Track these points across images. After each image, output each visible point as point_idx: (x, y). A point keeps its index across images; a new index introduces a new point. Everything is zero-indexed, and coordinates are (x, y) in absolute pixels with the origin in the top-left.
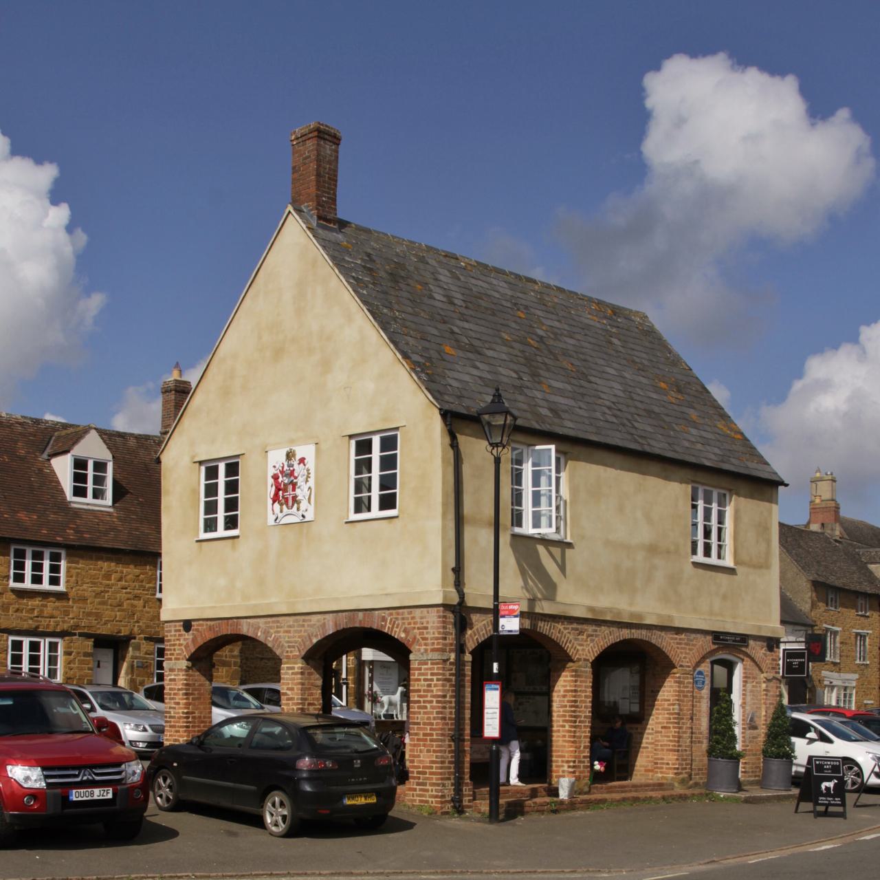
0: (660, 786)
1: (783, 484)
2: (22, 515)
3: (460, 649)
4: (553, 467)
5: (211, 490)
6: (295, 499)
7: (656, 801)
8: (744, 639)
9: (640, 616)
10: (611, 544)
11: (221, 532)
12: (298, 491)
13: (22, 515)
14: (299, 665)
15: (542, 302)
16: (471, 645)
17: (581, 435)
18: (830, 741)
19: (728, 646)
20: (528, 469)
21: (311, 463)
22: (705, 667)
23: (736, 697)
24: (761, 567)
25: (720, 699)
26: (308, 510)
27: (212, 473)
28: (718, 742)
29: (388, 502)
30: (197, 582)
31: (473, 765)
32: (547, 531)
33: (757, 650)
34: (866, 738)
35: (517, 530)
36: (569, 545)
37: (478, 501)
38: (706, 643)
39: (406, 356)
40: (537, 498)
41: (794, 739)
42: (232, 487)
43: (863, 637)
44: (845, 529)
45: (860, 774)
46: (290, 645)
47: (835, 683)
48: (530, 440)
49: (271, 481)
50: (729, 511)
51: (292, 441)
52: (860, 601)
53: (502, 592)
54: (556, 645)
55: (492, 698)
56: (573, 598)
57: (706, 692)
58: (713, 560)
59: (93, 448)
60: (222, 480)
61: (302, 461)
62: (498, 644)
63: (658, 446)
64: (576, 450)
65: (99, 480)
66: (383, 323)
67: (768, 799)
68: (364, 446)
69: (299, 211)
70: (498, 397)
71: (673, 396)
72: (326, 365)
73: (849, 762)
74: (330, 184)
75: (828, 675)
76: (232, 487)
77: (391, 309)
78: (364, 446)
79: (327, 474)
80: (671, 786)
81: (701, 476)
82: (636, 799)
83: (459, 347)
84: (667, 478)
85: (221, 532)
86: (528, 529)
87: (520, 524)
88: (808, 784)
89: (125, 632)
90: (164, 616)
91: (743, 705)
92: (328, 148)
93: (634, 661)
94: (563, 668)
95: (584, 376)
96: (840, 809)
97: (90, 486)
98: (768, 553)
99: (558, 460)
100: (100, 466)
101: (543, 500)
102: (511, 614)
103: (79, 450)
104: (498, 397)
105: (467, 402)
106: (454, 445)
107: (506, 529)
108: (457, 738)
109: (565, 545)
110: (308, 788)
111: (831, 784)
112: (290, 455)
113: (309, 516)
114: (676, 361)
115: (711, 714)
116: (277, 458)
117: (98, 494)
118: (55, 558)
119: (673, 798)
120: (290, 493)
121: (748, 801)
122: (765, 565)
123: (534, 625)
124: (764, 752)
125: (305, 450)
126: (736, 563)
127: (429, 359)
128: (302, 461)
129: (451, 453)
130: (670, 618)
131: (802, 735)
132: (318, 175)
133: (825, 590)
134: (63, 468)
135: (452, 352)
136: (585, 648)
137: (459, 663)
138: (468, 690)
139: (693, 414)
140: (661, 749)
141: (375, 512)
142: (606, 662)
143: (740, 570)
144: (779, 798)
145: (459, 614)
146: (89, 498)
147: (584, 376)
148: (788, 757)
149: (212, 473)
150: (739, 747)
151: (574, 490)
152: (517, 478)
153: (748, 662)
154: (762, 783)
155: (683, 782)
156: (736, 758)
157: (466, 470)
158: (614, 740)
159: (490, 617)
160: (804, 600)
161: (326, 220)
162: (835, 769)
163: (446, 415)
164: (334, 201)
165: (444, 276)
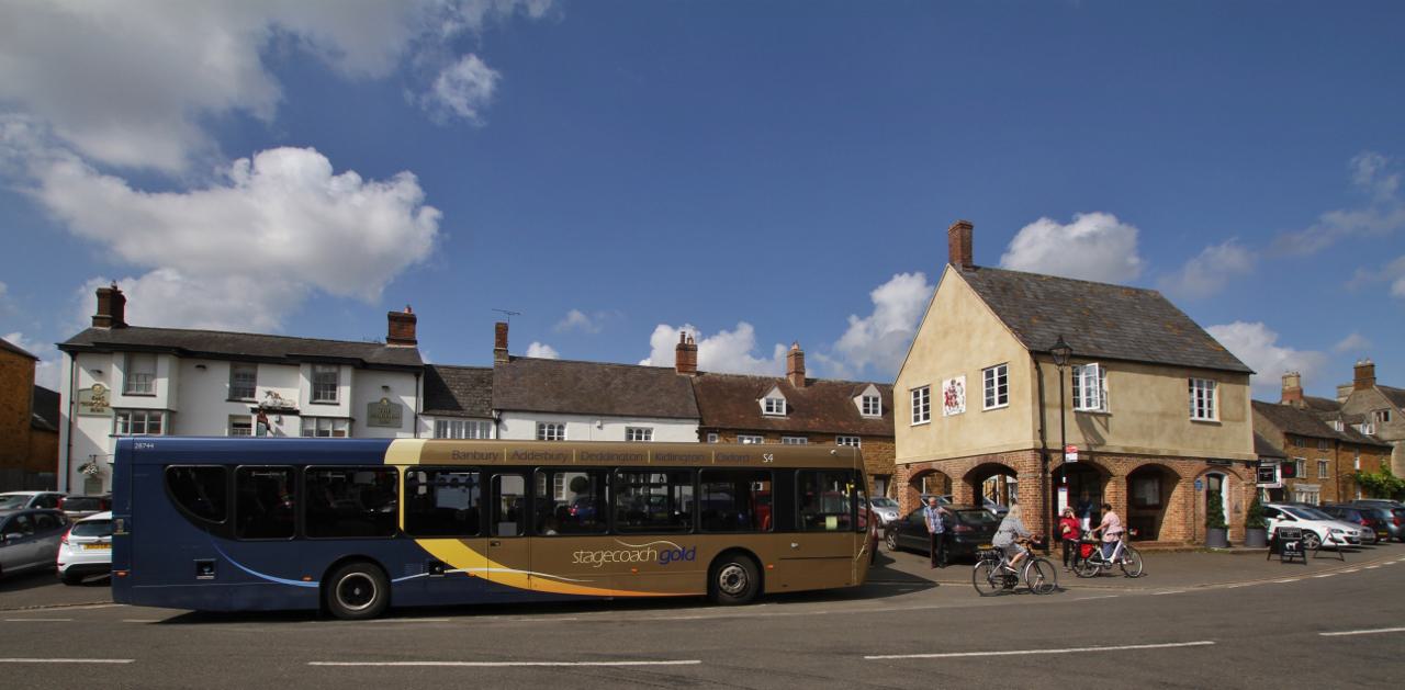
0: (1173, 544)
1: (1252, 372)
2: (841, 424)
3: (1045, 471)
4: (1097, 374)
5: (917, 402)
6: (956, 403)
7: (1171, 551)
8: (1229, 462)
9: (1156, 451)
10: (1134, 412)
11: (922, 421)
12: (958, 399)
13: (841, 424)
14: (961, 482)
15: (1091, 292)
16: (1051, 469)
17: (1115, 357)
18: (1295, 520)
19: (1218, 467)
20: (1082, 378)
21: (963, 386)
22: (1203, 478)
23: (1224, 495)
24: (1238, 421)
25: (1214, 498)
26: (963, 407)
27: (917, 394)
28: (1212, 520)
29: (1003, 400)
30: (912, 446)
31: (703, 514)
32: (1095, 408)
33: (1240, 469)
34: (1323, 518)
35: (1077, 409)
36: (1110, 415)
37: (1052, 395)
38: (1203, 465)
39: (1009, 326)
40: (1088, 394)
41: (1269, 519)
42: (926, 400)
43: (1324, 463)
44: (1308, 403)
45: (1318, 539)
46: (957, 472)
47: (1303, 489)
48: (1082, 362)
49: (944, 395)
50: (1215, 393)
51: (954, 375)
52: (1320, 443)
53: (1067, 441)
54: (1103, 467)
55: (1063, 496)
56: (1114, 443)
57: (1203, 492)
58: (1205, 418)
59: (872, 392)
60: (921, 397)
61: (959, 384)
62: (1068, 468)
63: (1165, 358)
64: (1110, 365)
65: (875, 406)
66: (997, 312)
67: (1248, 552)
68: (990, 374)
69: (953, 265)
70: (1061, 339)
71: (1175, 332)
72: (969, 337)
73: (1311, 533)
74: (1027, 285)
75: (1297, 486)
76: (926, 400)
77: (1001, 304)
78: (990, 374)
79: (971, 388)
80: (1181, 544)
81: (1194, 373)
82: (1157, 551)
83: (1040, 318)
84: (1171, 376)
85: (922, 421)
86: (1083, 408)
87: (1079, 406)
88: (1277, 544)
89: (888, 472)
90: (897, 462)
91: (1230, 499)
92: (967, 232)
93: (1153, 477)
94: (1109, 480)
95: (1118, 327)
96: (1302, 559)
97: (871, 408)
98: (1244, 413)
99: (1100, 372)
100: (875, 399)
101: (1093, 392)
102: (1072, 451)
103: (865, 393)
104: (1061, 339)
105: (1044, 346)
106: (1038, 368)
107: (1070, 408)
108: (1044, 516)
109: (1107, 415)
110: (958, 540)
111: (1294, 544)
112: (953, 382)
113: (964, 410)
114: (1177, 313)
115: (1207, 505)
116: (947, 385)
117: (875, 412)
118: (856, 441)
119: (1182, 550)
120: (953, 401)
121: (1233, 553)
122: (1243, 420)
123: (1091, 458)
124: (1246, 526)
125: (961, 379)
126: (1221, 419)
127: (1024, 327)
128: (959, 384)
129: (1036, 372)
130: (1177, 451)
131: (1274, 517)
132: (962, 246)
133: (1292, 437)
134: (859, 401)
135: (1036, 321)
136: (1122, 469)
137: (1044, 479)
138: (1050, 492)
139: (1189, 340)
140: (1174, 523)
141: (997, 405)
142: (1136, 479)
143: (1224, 423)
144: (1257, 552)
145: (1044, 453)
146: (871, 414)
147: (1118, 327)
148: (1265, 530)
149: (917, 394)
150: (1227, 522)
151: (1111, 386)
152: (1076, 382)
153: (1232, 474)
154: (1244, 543)
155: (1189, 541)
156: (1226, 528)
157: (1045, 380)
158: (1143, 523)
159: (1060, 455)
160: (1278, 442)
161: (967, 267)
162: (1296, 535)
163: (1031, 353)
164: (971, 257)
165: (1033, 286)
